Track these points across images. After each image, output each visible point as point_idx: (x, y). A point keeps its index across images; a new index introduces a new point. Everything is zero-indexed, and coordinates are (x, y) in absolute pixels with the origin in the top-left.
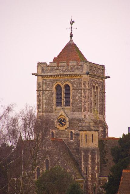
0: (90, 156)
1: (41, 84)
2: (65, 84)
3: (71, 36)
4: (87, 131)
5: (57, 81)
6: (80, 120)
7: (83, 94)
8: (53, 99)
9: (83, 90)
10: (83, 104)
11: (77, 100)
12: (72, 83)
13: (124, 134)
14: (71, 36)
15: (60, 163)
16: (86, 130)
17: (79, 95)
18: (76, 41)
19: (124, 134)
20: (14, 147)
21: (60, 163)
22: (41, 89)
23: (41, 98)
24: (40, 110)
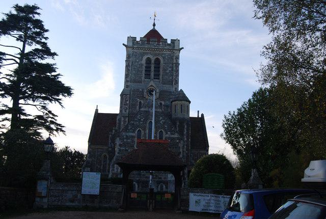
0: (186, 127)
1: (131, 55)
2: (155, 57)
3: (154, 25)
4: (183, 102)
5: (147, 54)
6: (170, 92)
7: (174, 68)
8: (142, 71)
9: (174, 65)
10: (174, 77)
11: (167, 74)
12: (164, 58)
13: (67, 91)
14: (154, 25)
15: (166, 126)
16: (182, 100)
17: (170, 69)
18: (156, 28)
19: (67, 91)
20: (28, 129)
21: (166, 126)
22: (131, 59)
23: (130, 69)
24: (128, 79)
